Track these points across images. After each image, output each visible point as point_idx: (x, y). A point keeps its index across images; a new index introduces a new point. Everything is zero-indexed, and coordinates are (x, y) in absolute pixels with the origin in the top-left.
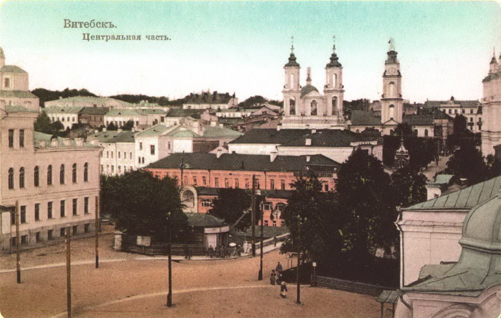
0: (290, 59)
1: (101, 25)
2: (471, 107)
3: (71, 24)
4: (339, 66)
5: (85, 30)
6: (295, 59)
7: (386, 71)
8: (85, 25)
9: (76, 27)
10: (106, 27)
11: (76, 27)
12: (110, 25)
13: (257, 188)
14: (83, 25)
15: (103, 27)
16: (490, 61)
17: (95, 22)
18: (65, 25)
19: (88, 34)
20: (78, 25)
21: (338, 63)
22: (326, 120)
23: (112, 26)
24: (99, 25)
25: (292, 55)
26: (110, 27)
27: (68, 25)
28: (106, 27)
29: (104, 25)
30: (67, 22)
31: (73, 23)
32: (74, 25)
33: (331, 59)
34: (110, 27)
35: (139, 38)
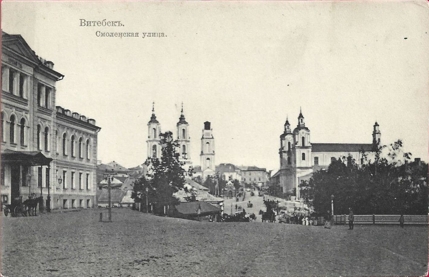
0: (152, 118)
1: (127, 34)
2: (348, 151)
3: (86, 23)
4: (186, 123)
5: (97, 28)
6: (156, 117)
7: (203, 135)
8: (98, 24)
9: (90, 25)
10: (115, 25)
11: (90, 25)
12: (119, 24)
13: (371, 157)
14: (96, 24)
15: (113, 25)
16: (200, 153)
17: (107, 21)
18: (81, 24)
19: (88, 25)
20: (92, 24)
21: (185, 121)
22: (213, 145)
23: (120, 24)
24: (109, 24)
25: (153, 115)
26: (119, 25)
27: (83, 24)
28: (115, 25)
29: (113, 23)
30: (83, 21)
31: (88, 22)
32: (88, 24)
33: (180, 119)
34: (119, 25)
35: (137, 34)
